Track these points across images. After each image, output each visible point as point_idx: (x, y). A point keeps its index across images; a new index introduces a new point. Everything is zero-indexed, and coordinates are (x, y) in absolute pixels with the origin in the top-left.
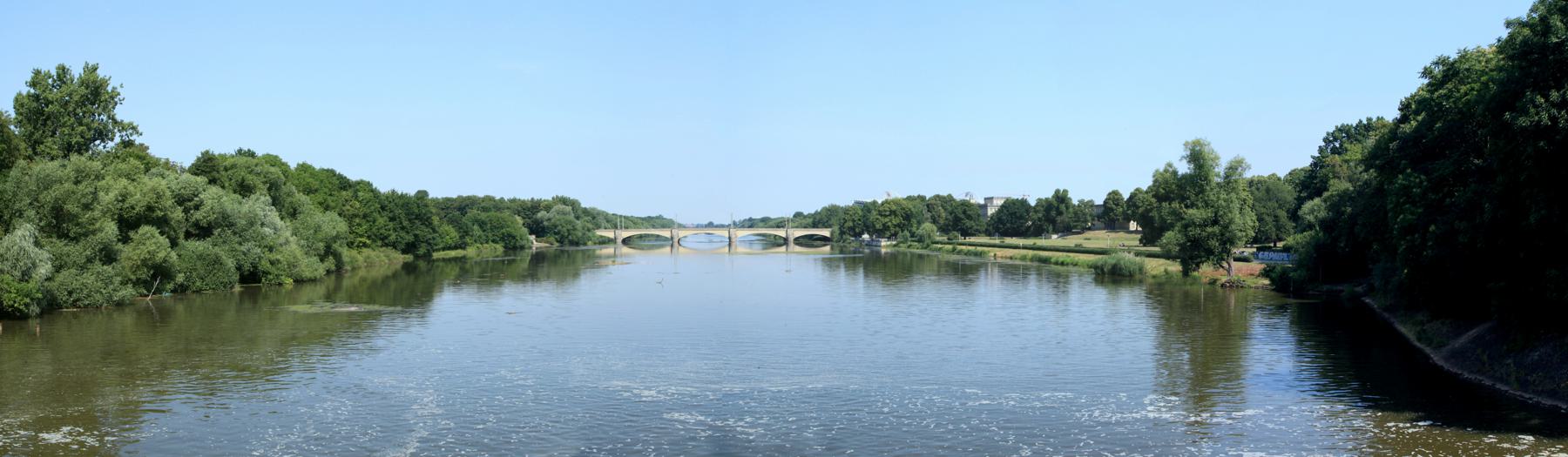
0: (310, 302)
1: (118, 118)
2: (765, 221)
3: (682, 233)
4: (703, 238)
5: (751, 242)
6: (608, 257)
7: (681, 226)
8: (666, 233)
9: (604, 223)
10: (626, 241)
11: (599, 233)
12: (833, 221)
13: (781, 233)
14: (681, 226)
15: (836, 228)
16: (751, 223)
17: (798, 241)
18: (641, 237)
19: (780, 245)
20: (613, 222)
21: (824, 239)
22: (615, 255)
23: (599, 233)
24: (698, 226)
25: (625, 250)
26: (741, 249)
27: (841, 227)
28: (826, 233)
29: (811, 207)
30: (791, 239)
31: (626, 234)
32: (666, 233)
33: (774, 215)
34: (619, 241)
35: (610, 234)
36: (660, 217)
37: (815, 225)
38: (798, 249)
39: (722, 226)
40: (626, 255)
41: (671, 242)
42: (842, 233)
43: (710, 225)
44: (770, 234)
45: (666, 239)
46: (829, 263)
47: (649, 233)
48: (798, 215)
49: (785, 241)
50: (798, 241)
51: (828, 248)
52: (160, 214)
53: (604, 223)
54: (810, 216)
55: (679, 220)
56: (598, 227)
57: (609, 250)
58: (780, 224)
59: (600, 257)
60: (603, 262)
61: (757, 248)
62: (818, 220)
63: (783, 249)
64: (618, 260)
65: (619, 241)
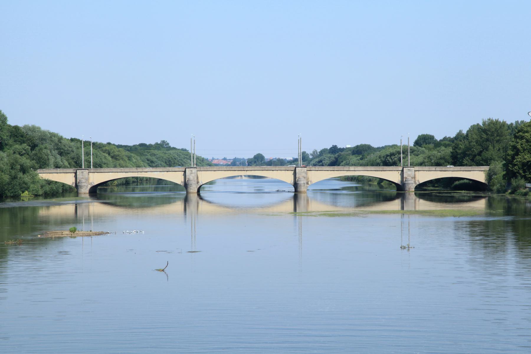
0: (344, 207)
1: (201, 195)
2: (362, 153)
3: (205, 176)
4: (246, 185)
5: (335, 193)
6: (63, 222)
7: (203, 163)
8: (175, 176)
9: (53, 157)
10: (98, 192)
11: (45, 175)
12: (492, 152)
13: (392, 175)
14: (203, 163)
15: (498, 166)
16: (335, 157)
17: (425, 191)
18: (126, 183)
19: (389, 199)
20: (71, 153)
21: (475, 187)
22: (76, 220)
23: (45, 175)
24: (235, 163)
25: (97, 208)
26: (317, 205)
27: (509, 163)
28: (478, 175)
29: (447, 127)
30: (411, 186)
31: (97, 178)
32: (175, 176)
33: (377, 141)
34: (85, 190)
35: (66, 178)
36: (162, 146)
37: (456, 160)
38: (423, 205)
39: (280, 163)
40: (99, 218)
41: (183, 192)
42: (510, 175)
43: (258, 160)
44: (369, 177)
45: (174, 187)
46: (484, 232)
47: (143, 176)
48: (424, 141)
49: (399, 191)
50: (425, 191)
51: (481, 204)
52: (476, 229)
53: (53, 157)
54: (446, 142)
55: (200, 151)
56: (43, 164)
57: (65, 209)
58: (390, 158)
59: (46, 222)
60: (54, 232)
61: (347, 203)
62: (460, 150)
63: (395, 205)
64: (83, 228)
65: (85, 190)
